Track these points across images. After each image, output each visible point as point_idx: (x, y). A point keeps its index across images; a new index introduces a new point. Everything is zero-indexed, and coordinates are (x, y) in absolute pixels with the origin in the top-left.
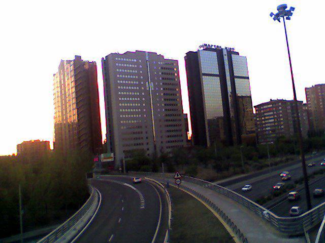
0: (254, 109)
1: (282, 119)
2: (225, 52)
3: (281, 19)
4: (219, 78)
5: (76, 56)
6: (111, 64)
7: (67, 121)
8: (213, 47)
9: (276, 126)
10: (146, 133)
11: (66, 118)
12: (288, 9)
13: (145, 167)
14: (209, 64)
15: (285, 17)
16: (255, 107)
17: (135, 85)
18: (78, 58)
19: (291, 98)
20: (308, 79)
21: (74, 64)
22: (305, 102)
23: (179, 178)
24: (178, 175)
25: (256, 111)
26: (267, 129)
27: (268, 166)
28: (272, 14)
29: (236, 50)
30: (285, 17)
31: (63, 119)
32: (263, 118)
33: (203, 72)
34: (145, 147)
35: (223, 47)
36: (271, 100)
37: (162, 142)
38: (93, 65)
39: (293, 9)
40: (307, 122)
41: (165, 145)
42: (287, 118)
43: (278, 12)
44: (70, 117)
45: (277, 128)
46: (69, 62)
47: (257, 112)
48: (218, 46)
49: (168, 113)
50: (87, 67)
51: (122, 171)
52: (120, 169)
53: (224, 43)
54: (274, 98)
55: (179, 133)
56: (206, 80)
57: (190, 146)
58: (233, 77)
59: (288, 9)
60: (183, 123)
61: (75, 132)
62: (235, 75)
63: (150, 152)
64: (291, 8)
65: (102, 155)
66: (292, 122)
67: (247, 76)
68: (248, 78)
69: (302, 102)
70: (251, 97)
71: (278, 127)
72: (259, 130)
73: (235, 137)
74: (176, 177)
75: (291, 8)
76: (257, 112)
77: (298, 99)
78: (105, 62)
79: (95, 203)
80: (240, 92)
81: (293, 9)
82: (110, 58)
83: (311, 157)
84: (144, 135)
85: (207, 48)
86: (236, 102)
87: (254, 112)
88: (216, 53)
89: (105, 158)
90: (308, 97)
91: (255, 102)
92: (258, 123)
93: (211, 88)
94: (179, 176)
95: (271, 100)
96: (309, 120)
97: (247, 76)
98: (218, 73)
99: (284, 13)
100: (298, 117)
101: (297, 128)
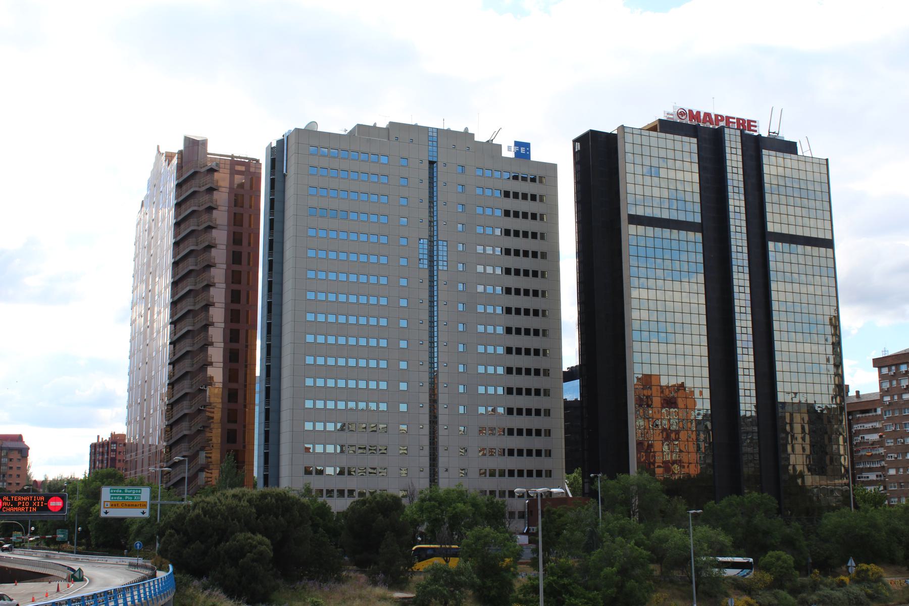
4: (699, 236)
6: (291, 168)
14: (661, 183)
17: (378, 333)
18: (194, 146)
21: (180, 167)
46: (169, 157)
49: (514, 282)
55: (536, 443)
58: (760, 237)
62: (770, 228)
68: (828, 244)
72: (892, 472)
82: (292, 141)
88: (695, 140)
89: (114, 505)
97: (829, 237)
98: (698, 219)
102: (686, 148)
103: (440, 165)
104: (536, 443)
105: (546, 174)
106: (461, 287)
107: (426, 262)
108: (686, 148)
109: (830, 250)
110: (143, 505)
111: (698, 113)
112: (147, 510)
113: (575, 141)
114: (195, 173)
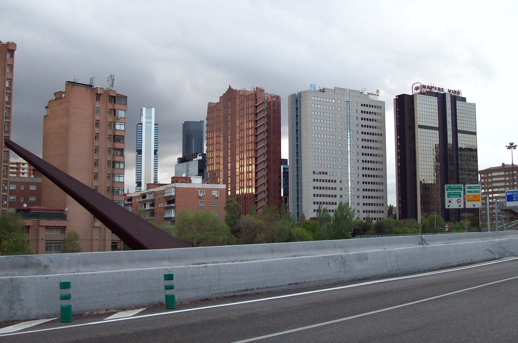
9: (491, 193)
10: (341, 196)
14: (426, 112)
16: (482, 172)
25: (481, 178)
29: (463, 95)
32: (490, 190)
35: (446, 91)
36: (503, 164)
47: (483, 181)
48: (439, 89)
53: (447, 85)
56: (420, 133)
62: (458, 129)
68: (475, 134)
76: (483, 181)
83: (505, 180)
85: (429, 91)
90: (497, 257)
95: (503, 164)
105: (381, 106)
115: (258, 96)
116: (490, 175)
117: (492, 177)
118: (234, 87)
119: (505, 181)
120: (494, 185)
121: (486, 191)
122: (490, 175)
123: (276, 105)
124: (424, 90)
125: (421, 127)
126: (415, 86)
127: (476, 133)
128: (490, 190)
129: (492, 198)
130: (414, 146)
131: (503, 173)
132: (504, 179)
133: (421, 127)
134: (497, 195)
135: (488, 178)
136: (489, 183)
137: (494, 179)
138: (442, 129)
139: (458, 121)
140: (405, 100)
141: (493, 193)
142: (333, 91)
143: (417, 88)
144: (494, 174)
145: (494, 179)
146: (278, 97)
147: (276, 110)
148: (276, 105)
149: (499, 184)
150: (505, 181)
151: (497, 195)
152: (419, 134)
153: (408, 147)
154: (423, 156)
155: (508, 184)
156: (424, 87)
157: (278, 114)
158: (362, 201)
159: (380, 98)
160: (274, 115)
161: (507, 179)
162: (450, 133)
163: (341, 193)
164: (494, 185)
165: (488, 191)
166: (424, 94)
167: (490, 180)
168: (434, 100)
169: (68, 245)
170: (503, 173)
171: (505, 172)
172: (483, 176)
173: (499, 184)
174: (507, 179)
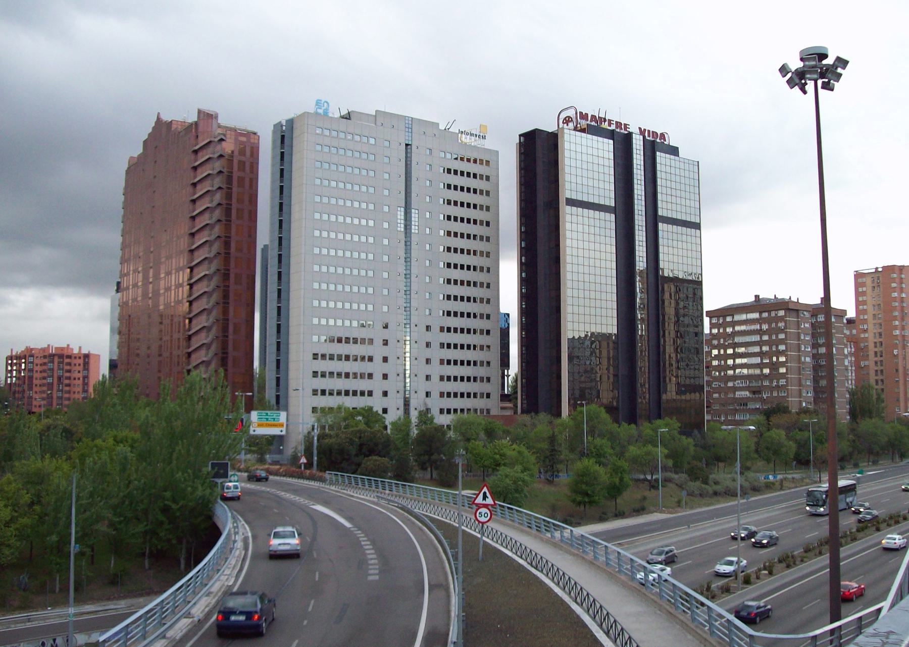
0: (706, 320)
1: (782, 359)
2: (638, 144)
3: (810, 86)
5: (200, 112)
7: (156, 305)
8: (605, 125)
11: (156, 293)
12: (829, 61)
13: (374, 461)
14: (586, 166)
15: (820, 82)
16: (710, 314)
19: (813, 297)
20: (861, 250)
22: (851, 314)
23: (486, 506)
24: (485, 497)
25: (712, 326)
26: (739, 394)
27: (734, 495)
28: (784, 70)
30: (820, 82)
31: (145, 295)
32: (730, 351)
33: (568, 195)
34: (377, 403)
36: (757, 297)
37: (428, 394)
38: (248, 144)
39: (842, 62)
40: (851, 375)
41: (436, 404)
42: (799, 346)
43: (801, 64)
44: (168, 289)
45: (766, 383)
47: (715, 331)
48: (618, 124)
50: (228, 147)
51: (309, 465)
52: (303, 460)
54: (767, 294)
57: (508, 413)
58: (654, 219)
59: (829, 61)
60: (494, 340)
61: (176, 336)
62: (660, 213)
63: (390, 418)
64: (838, 59)
65: (254, 415)
66: (808, 359)
67: (693, 219)
68: (697, 226)
69: (844, 312)
70: (700, 283)
71: (771, 382)
72: (716, 395)
73: (644, 397)
74: (480, 500)
75: (838, 59)
76: (715, 331)
77: (835, 304)
78: (285, 137)
79: (238, 551)
80: (672, 263)
81: (842, 62)
83: (761, 330)
84: (377, 368)
85: (594, 126)
86: (658, 300)
87: (707, 330)
89: (260, 425)
91: (712, 300)
92: (715, 363)
93: (587, 250)
94: (489, 501)
95: (757, 297)
96: (858, 368)
99: (817, 70)
100: (829, 356)
101: (824, 392)
102: (606, 148)
103: (414, 148)
104: (481, 371)
105: (488, 161)
106: (428, 247)
107: (403, 226)
108: (606, 148)
109: (698, 231)
110: (282, 425)
111: (587, 114)
112: (284, 429)
113: (520, 136)
114: (210, 142)
115: (200, 129)
116: (729, 319)
117: (733, 324)
118: (166, 117)
119: (760, 332)
120: (738, 339)
121: (722, 352)
122: (729, 319)
123: (248, 153)
124: (584, 123)
125: (571, 202)
126: (563, 116)
127: (700, 224)
128: (730, 351)
129: (734, 367)
130: (558, 245)
131: (755, 315)
132: (758, 327)
133: (571, 202)
134: (744, 361)
135: (725, 325)
136: (726, 336)
137: (737, 328)
138: (623, 210)
139: (659, 196)
140: (539, 142)
141: (735, 356)
142: (373, 119)
143: (567, 120)
144: (737, 318)
145: (737, 328)
146: (252, 135)
147: (248, 165)
148: (248, 153)
149: (748, 339)
150: (760, 332)
151: (744, 361)
152: (568, 218)
153: (542, 249)
154: (575, 270)
155: (766, 338)
156: (584, 116)
157: (252, 172)
158: (437, 370)
159: (488, 144)
160: (241, 174)
161: (765, 327)
162: (640, 220)
163: (428, 353)
164: (738, 339)
165: (725, 351)
166: (583, 131)
167: (729, 330)
168: (606, 146)
169: (868, 374)
170: (755, 315)
171: (761, 313)
172: (714, 321)
173: (748, 339)
174: (765, 327)
